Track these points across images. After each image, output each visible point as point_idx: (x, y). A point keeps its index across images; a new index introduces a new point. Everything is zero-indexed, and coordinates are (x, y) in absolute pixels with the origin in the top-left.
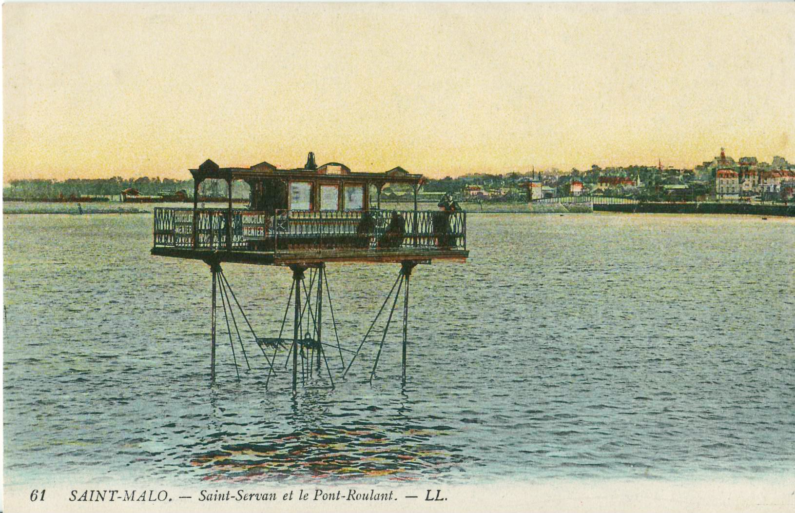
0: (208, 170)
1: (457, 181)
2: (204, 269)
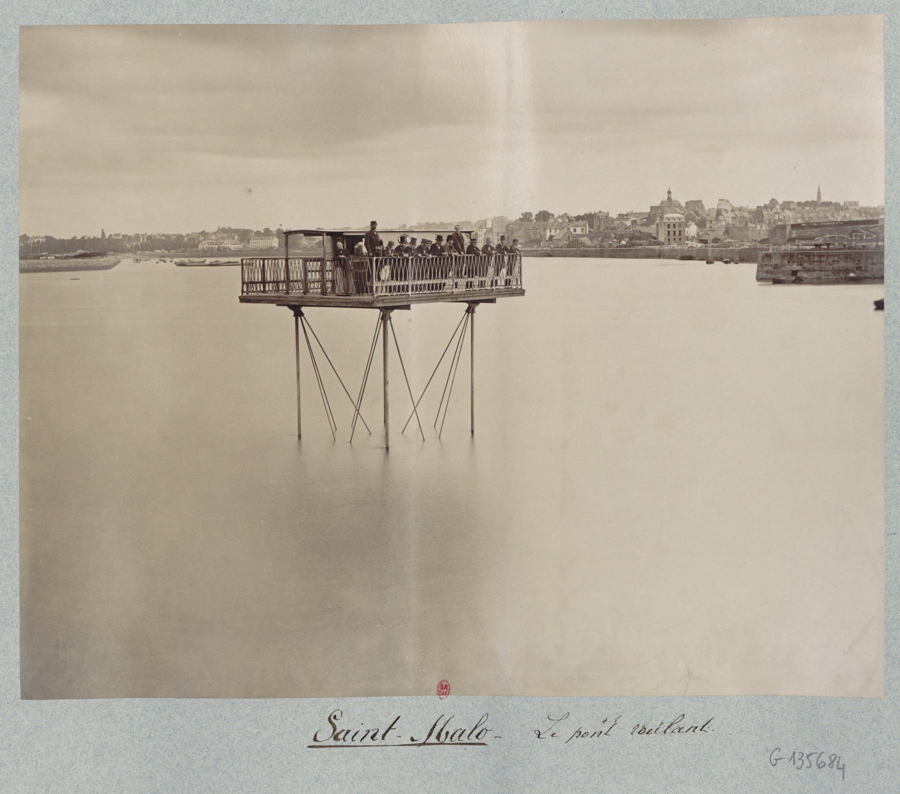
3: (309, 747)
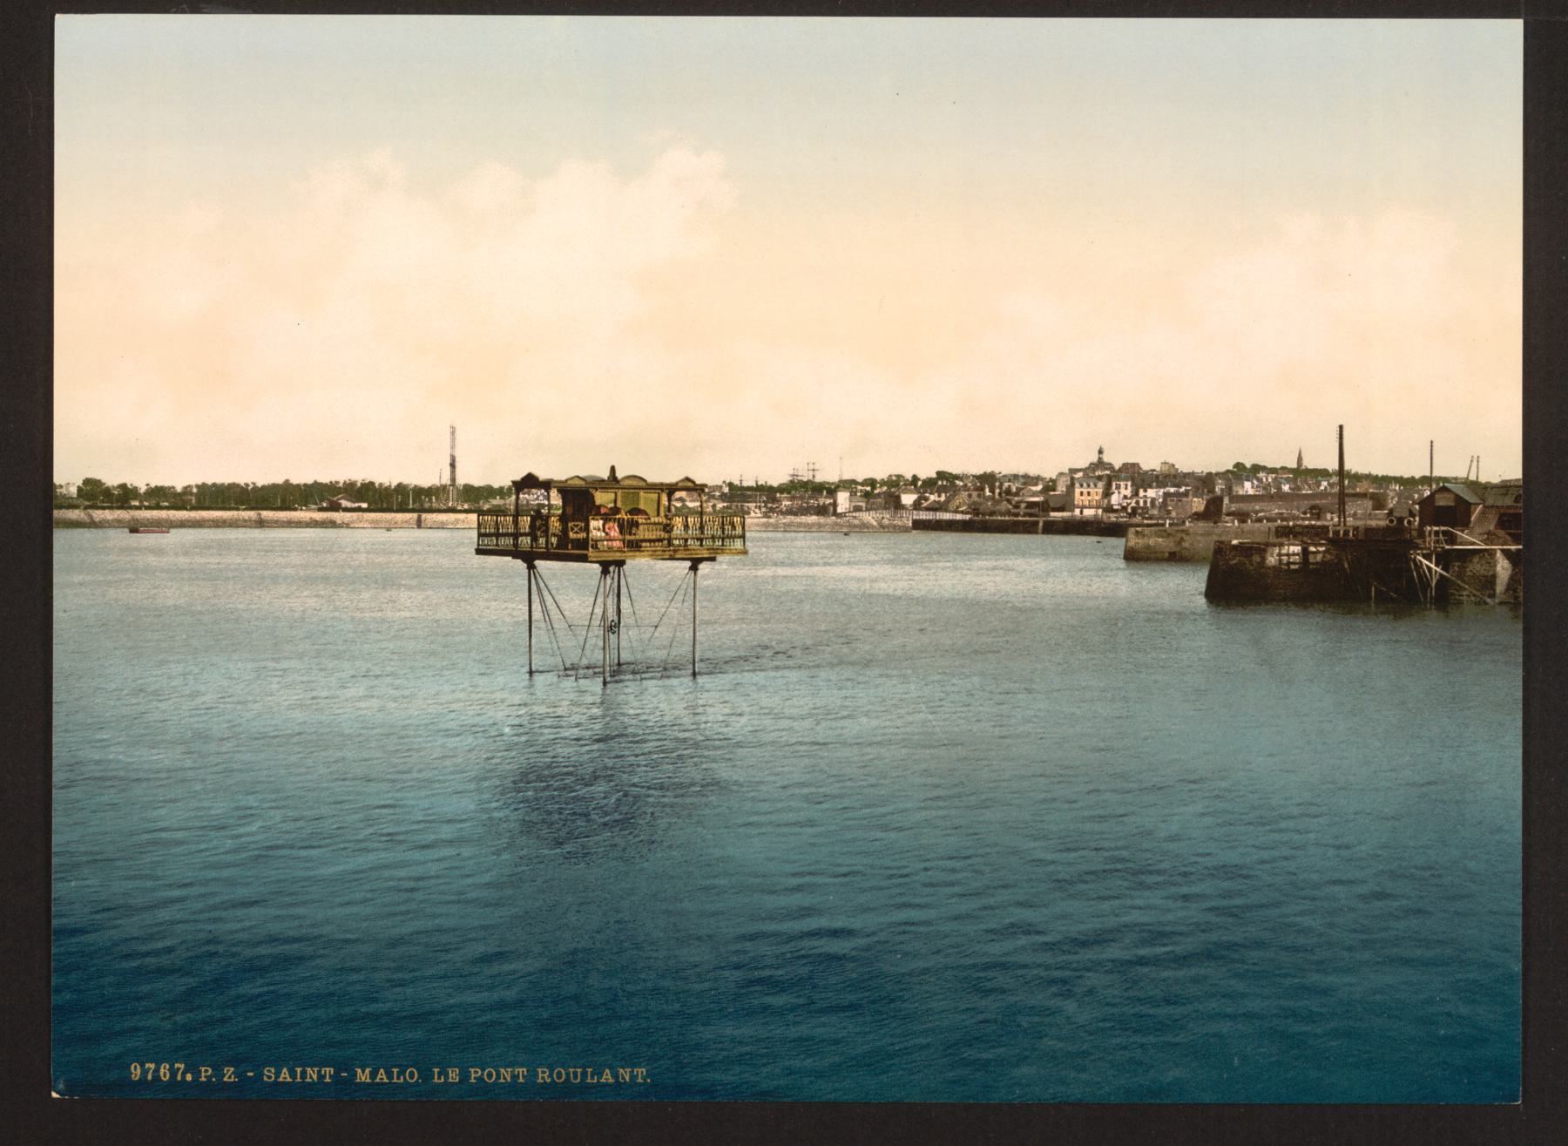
0: (529, 482)
1: (479, 489)
2: (520, 565)
3: (1341, 427)
